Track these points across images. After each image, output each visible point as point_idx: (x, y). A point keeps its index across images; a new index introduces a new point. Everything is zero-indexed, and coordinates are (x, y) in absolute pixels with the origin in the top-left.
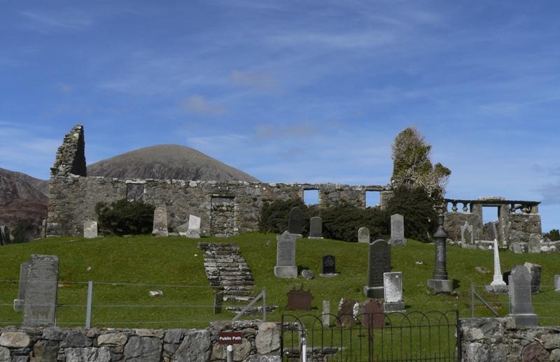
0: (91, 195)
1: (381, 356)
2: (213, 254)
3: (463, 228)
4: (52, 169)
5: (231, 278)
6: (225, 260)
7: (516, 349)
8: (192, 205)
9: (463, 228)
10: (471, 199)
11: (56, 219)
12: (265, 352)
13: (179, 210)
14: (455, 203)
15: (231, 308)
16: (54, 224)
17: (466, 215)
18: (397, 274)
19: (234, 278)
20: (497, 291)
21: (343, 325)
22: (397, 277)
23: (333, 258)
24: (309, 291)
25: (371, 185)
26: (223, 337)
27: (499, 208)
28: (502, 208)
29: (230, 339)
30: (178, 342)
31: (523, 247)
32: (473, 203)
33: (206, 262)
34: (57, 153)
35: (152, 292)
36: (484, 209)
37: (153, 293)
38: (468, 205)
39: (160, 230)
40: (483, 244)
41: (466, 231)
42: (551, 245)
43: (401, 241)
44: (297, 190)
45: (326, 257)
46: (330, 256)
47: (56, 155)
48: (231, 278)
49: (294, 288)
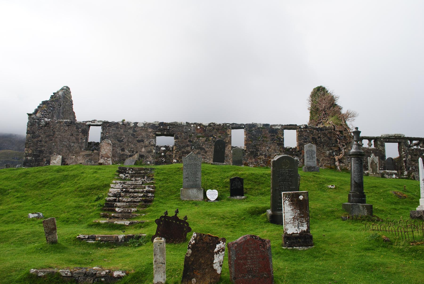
8: (139, 141)
9: (370, 160)
10: (376, 135)
11: (31, 154)
13: (128, 145)
16: (29, 158)
17: (371, 150)
20: (309, 124)
24: (186, 218)
25: (289, 124)
27: (399, 143)
28: (402, 144)
32: (376, 139)
33: (112, 183)
35: (30, 214)
37: (31, 216)
38: (372, 142)
40: (387, 174)
43: (314, 167)
49: (166, 213)
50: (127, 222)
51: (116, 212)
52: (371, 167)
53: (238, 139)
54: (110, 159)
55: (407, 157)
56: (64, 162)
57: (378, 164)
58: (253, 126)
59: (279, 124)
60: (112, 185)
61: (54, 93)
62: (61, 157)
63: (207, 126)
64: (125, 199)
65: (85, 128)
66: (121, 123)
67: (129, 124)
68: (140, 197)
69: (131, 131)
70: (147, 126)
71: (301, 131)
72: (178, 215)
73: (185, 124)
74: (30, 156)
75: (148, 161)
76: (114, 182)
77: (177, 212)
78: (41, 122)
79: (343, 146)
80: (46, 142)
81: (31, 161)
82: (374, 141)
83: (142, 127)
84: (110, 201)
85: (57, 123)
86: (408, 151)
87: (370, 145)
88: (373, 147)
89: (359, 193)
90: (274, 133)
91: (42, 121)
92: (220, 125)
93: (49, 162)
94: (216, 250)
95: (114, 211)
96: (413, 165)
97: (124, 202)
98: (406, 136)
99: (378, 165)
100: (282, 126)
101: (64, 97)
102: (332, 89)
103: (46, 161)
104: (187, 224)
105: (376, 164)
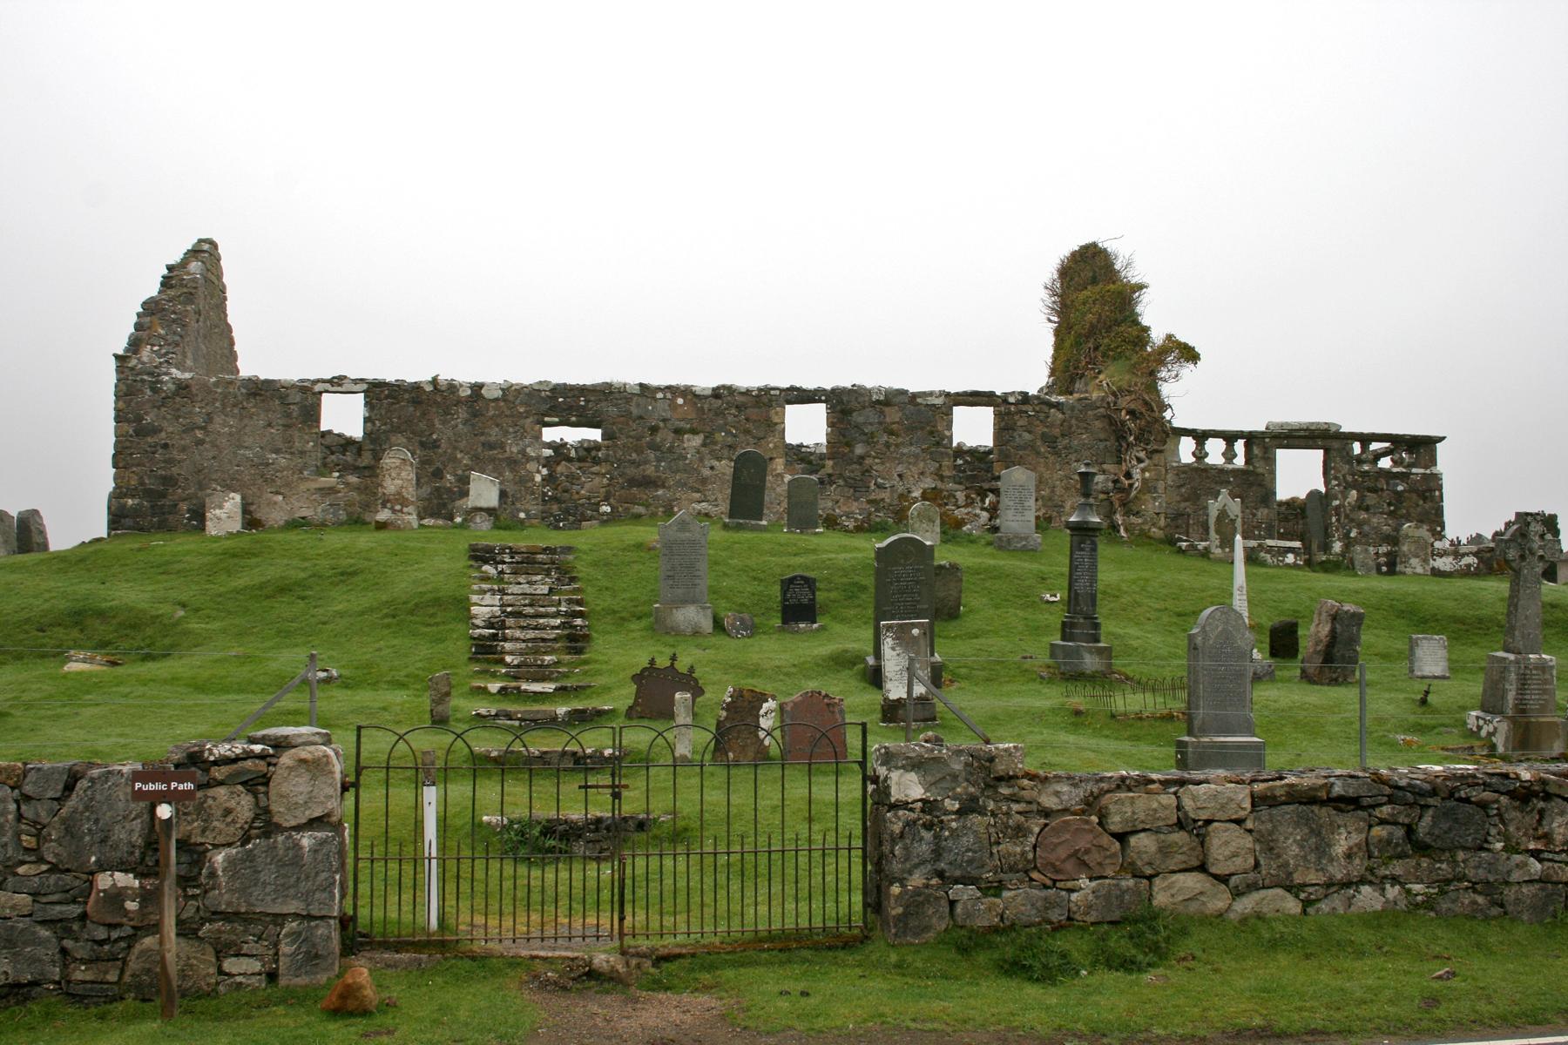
0: (224, 425)
1: (752, 839)
2: (502, 572)
3: (1214, 507)
4: (117, 357)
5: (531, 634)
6: (526, 588)
7: (1020, 832)
9: (1214, 507)
10: (1247, 428)
12: (293, 823)
14: (1201, 437)
15: (483, 711)
16: (130, 502)
18: (914, 625)
19: (537, 634)
21: (731, 755)
22: (915, 632)
23: (809, 583)
24: (692, 670)
26: (145, 782)
28: (1333, 454)
29: (163, 787)
30: (58, 795)
31: (1383, 560)
32: (1251, 438)
34: (139, 315)
36: (1281, 454)
38: (1239, 446)
39: (394, 511)
40: (1270, 550)
41: (1223, 514)
42: (1463, 555)
43: (1026, 539)
44: (769, 405)
45: (792, 580)
46: (803, 578)
47: (135, 319)
48: (531, 634)
49: (652, 662)
50: (549, 687)
51: (508, 665)
52: (1217, 532)
53: (806, 427)
54: (411, 509)
55: (1345, 498)
56: (251, 522)
57: (1239, 521)
58: (857, 392)
59: (937, 388)
60: (474, 598)
61: (170, 268)
62: (238, 497)
63: (706, 397)
64: (518, 634)
65: (299, 402)
66: (429, 388)
67: (452, 387)
68: (553, 628)
69: (462, 413)
70: (512, 395)
71: (1009, 413)
72: (678, 665)
73: (637, 390)
74: (133, 497)
75: (519, 511)
76: (475, 587)
77: (674, 658)
78: (161, 382)
79: (1140, 460)
80: (184, 449)
81: (136, 512)
82: (1246, 445)
83: (496, 400)
84: (481, 637)
85: (216, 384)
86: (1349, 478)
87: (1229, 455)
88: (1240, 461)
89: (1081, 617)
90: (922, 416)
91: (166, 378)
92: (748, 392)
93: (199, 516)
94: (762, 712)
95: (502, 662)
96: (1365, 522)
97: (517, 640)
98: (1347, 428)
99: (1239, 523)
100: (948, 395)
101: (206, 279)
102: (1136, 258)
103: (189, 511)
104: (696, 680)
105: (1233, 521)
